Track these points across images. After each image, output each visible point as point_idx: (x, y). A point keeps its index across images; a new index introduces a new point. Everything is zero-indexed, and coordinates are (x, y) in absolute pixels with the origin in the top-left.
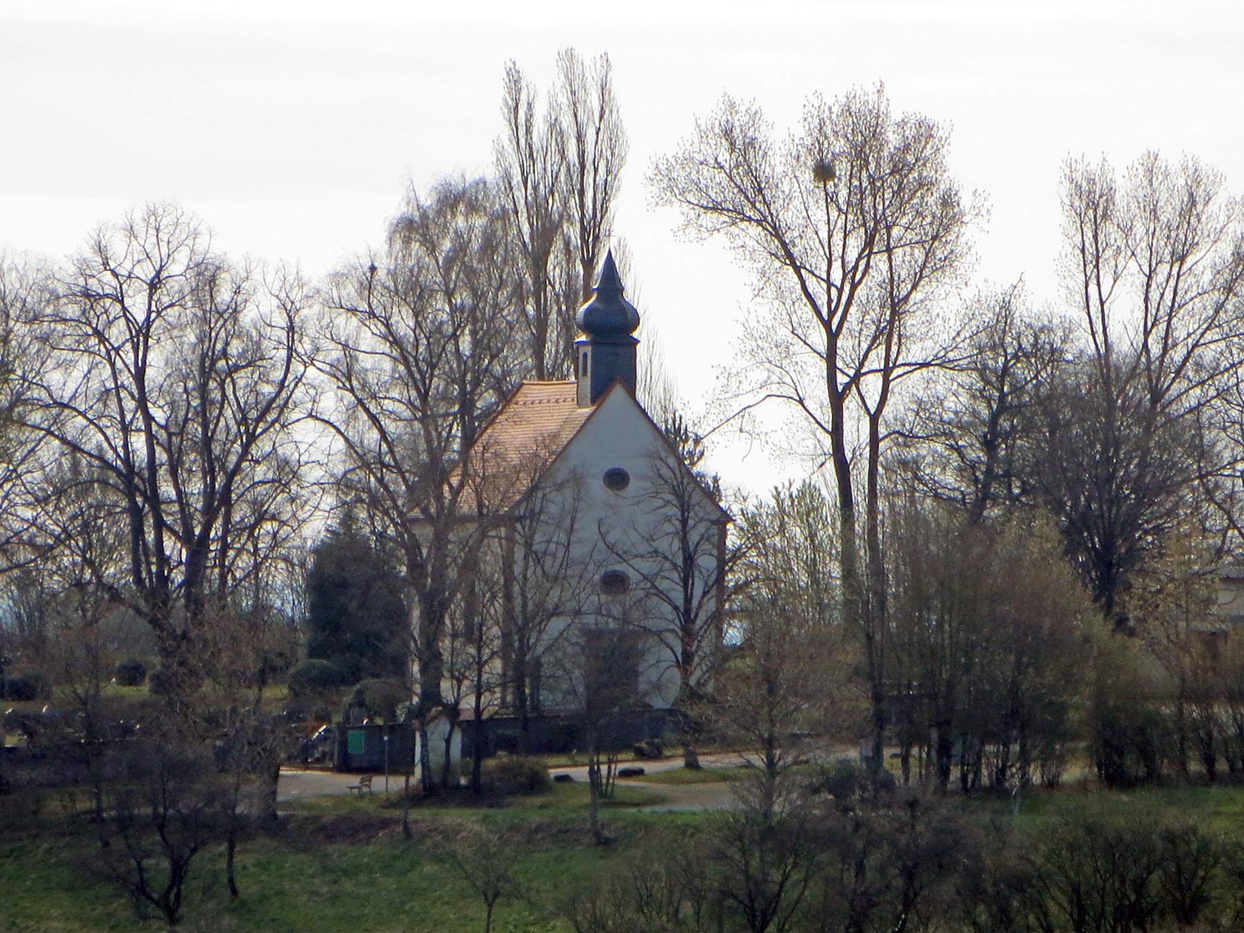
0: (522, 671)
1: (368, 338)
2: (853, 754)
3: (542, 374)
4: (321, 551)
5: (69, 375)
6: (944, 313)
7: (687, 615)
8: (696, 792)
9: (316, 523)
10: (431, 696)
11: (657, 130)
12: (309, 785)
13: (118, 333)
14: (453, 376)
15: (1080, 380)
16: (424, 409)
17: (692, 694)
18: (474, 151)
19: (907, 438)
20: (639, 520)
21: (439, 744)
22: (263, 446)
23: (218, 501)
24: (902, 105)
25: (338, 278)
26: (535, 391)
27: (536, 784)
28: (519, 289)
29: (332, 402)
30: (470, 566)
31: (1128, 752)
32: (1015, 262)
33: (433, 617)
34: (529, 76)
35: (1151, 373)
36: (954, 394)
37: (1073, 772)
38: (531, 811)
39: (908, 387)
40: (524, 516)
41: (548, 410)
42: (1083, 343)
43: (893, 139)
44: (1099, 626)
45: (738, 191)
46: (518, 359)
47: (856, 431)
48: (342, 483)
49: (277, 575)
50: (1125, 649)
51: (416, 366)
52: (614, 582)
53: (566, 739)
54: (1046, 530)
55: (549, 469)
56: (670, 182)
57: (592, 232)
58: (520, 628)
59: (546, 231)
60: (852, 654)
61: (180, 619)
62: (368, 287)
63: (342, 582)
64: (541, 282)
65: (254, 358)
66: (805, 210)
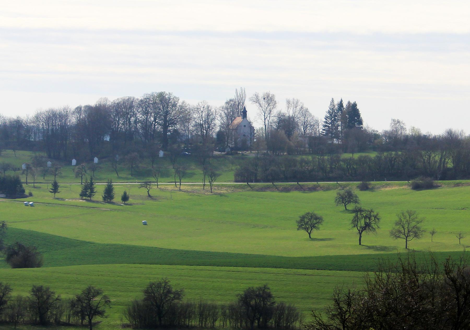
0: (236, 143)
1: (223, 113)
2: (265, 151)
3: (238, 116)
4: (218, 132)
5: (195, 116)
6: (275, 112)
7: (251, 139)
8: (251, 154)
9: (218, 129)
10: (228, 145)
11: (249, 94)
12: (216, 153)
13: (200, 112)
14: (230, 117)
15: (287, 118)
16: (227, 119)
17: (251, 146)
18: (233, 96)
19: (271, 123)
20: (247, 130)
21: (228, 150)
22: (213, 122)
23: (209, 127)
24: (271, 93)
25: (220, 107)
26: (238, 118)
27: (237, 153)
28: (236, 109)
29: (219, 118)
30: (231, 134)
31: (290, 151)
32: (282, 108)
33: (228, 138)
34: (238, 90)
35: (293, 118)
36: (276, 119)
37: (285, 154)
38: (236, 156)
39: (271, 118)
40: (236, 129)
41: (239, 120)
42: (288, 115)
43: (270, 96)
44: (288, 140)
45: (257, 100)
46: (236, 115)
47: (267, 122)
48: (220, 126)
49: (214, 134)
50: (420, 296)
51: (227, 115)
52: (244, 135)
53: (240, 149)
54: (283, 132)
55: (239, 125)
56: (251, 99)
57: (243, 103)
58: (236, 139)
59: (239, 104)
60: (265, 143)
61: (206, 138)
62: (223, 108)
63: (220, 134)
64: (238, 108)
65: (212, 114)
66: (262, 102)
